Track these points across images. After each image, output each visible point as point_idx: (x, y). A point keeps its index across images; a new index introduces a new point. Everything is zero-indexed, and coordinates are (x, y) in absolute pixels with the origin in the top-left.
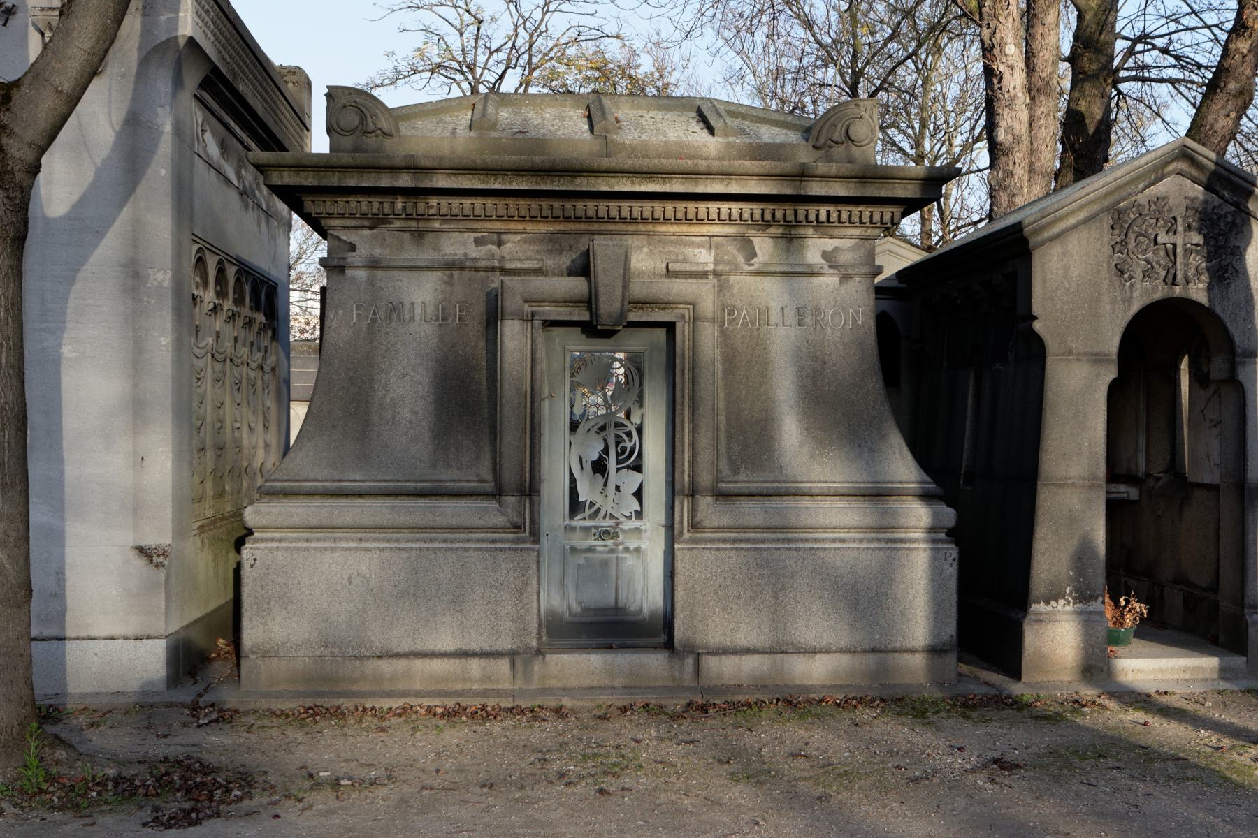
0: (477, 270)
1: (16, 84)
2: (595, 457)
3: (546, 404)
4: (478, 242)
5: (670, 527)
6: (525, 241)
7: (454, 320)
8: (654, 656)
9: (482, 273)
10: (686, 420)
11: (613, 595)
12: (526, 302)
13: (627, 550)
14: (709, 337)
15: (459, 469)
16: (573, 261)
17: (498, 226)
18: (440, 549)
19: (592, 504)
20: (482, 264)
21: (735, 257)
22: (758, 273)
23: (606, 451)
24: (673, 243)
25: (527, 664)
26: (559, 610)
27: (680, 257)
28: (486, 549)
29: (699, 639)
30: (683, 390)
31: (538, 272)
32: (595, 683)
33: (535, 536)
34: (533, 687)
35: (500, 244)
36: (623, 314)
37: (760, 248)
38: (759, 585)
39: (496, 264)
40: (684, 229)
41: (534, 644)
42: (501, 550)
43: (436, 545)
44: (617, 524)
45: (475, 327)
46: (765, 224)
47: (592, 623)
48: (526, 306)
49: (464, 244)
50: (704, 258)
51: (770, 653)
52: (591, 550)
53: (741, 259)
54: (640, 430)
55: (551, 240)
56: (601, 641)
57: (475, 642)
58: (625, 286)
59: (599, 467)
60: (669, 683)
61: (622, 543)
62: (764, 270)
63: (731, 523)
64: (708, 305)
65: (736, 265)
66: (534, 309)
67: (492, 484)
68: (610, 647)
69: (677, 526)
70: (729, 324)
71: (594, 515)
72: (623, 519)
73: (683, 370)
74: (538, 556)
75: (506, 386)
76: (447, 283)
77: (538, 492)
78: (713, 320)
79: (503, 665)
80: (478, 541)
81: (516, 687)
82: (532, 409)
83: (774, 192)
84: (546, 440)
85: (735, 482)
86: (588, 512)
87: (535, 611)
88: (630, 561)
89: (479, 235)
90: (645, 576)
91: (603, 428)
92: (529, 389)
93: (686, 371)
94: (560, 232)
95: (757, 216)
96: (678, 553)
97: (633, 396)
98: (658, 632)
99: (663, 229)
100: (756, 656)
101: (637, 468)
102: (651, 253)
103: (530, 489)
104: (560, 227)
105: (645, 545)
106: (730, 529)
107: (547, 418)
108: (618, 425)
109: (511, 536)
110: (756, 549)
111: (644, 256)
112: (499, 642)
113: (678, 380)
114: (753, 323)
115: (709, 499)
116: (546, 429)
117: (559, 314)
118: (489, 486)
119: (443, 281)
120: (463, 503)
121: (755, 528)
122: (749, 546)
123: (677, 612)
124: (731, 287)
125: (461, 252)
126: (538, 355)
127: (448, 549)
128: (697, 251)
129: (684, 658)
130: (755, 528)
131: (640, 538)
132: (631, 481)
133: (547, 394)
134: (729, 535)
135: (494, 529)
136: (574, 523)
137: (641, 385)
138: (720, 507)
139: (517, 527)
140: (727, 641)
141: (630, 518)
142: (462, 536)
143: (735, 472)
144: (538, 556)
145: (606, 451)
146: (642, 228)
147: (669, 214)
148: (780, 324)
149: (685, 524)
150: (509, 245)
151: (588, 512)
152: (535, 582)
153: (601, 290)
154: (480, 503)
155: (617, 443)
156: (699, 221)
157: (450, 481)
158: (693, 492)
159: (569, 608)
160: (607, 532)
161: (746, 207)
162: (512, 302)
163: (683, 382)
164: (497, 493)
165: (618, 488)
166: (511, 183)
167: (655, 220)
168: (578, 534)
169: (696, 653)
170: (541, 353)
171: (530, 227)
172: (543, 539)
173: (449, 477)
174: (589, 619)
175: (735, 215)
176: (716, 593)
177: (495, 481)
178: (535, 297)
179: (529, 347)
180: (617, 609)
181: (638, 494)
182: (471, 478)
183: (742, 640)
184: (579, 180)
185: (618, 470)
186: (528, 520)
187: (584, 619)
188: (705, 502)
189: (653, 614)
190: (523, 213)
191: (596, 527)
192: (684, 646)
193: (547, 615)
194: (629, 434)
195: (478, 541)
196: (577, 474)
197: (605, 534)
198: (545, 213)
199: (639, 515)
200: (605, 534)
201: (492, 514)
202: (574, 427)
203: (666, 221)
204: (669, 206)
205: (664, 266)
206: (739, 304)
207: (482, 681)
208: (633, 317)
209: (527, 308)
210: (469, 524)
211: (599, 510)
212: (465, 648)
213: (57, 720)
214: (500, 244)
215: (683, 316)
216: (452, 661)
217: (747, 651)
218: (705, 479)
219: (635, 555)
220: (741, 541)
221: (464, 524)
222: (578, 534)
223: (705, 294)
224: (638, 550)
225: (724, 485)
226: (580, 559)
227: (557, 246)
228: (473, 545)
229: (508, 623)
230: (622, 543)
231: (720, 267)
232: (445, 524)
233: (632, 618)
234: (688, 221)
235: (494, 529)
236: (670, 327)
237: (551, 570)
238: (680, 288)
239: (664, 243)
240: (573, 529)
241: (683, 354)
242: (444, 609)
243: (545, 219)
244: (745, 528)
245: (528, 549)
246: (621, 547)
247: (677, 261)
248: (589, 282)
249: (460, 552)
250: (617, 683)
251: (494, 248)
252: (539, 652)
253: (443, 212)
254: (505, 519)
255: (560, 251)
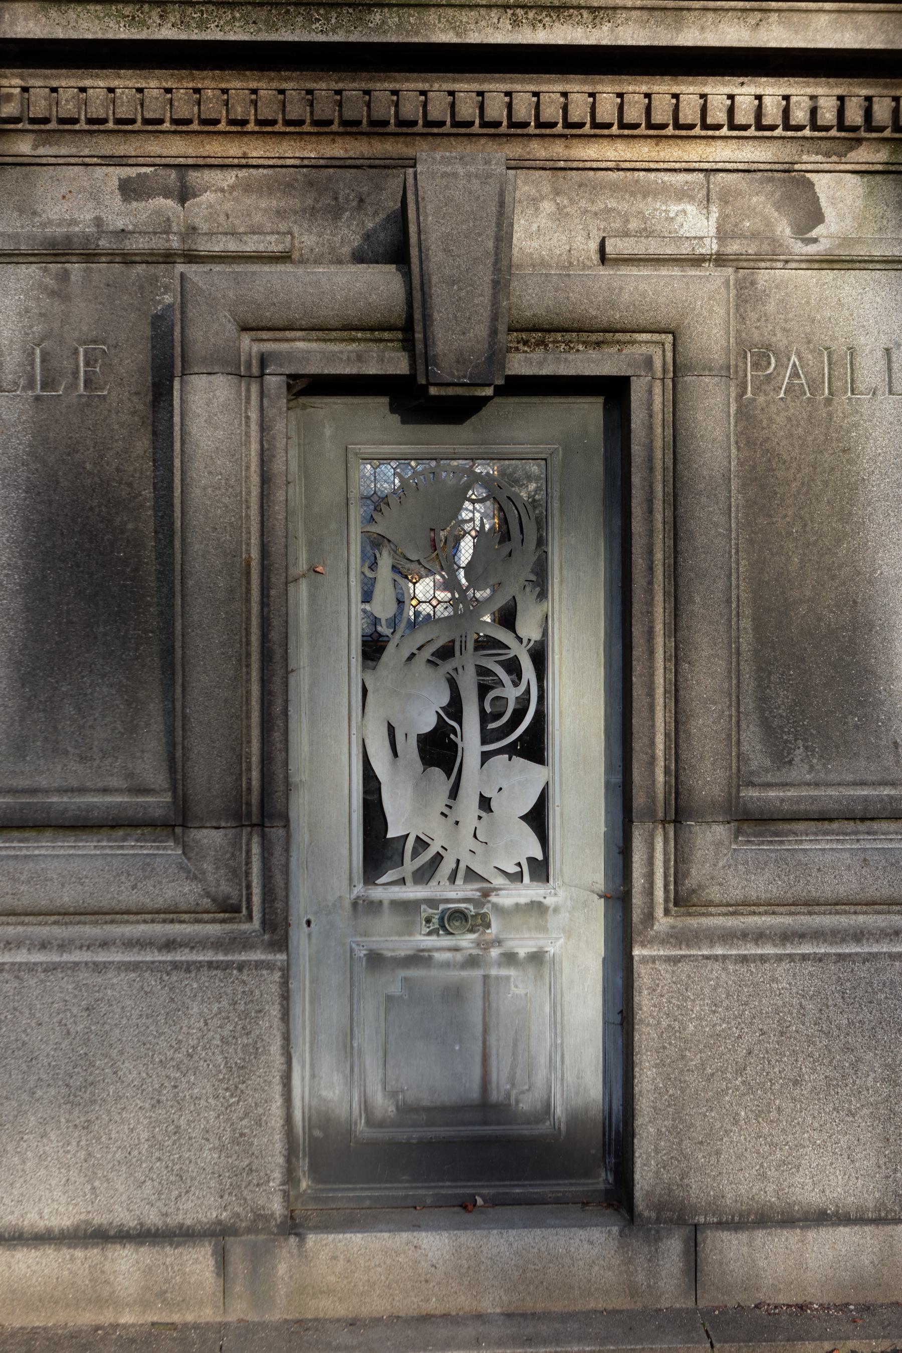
0: (128, 259)
1: (514, 631)
2: (428, 724)
3: (302, 590)
4: (130, 190)
5: (619, 898)
6: (247, 188)
7: (74, 385)
8: (582, 1234)
9: (140, 269)
10: (659, 628)
11: (477, 1073)
12: (245, 329)
13: (510, 958)
14: (713, 413)
15: (82, 759)
16: (367, 237)
17: (178, 148)
18: (31, 968)
19: (422, 844)
20: (140, 244)
21: (768, 224)
22: (830, 262)
23: (455, 709)
24: (614, 188)
25: (259, 1259)
26: (341, 1112)
27: (633, 225)
28: (151, 966)
29: (698, 1189)
30: (650, 552)
31: (284, 258)
32: (433, 1306)
33: (277, 931)
34: (275, 1316)
35: (184, 195)
36: (495, 355)
37: (833, 202)
38: (848, 1049)
39: (175, 243)
40: (643, 151)
41: (277, 1207)
42: (188, 967)
43: (21, 956)
44: (486, 894)
45: (123, 399)
46: (848, 134)
47: (428, 1145)
48: (246, 340)
49: (95, 196)
50: (696, 224)
51: (878, 1221)
52: (419, 959)
53: (784, 229)
54: (539, 656)
55: (311, 184)
56: (448, 1189)
57: (125, 1202)
58: (500, 285)
59: (439, 750)
60: (621, 1303)
61: (499, 942)
62: (843, 252)
63: (776, 891)
64: (712, 330)
65: (774, 241)
66: (268, 347)
67: (167, 798)
68: (466, 1205)
69: (637, 900)
70: (757, 390)
71: (426, 874)
72: (499, 881)
73: (650, 501)
74: (285, 982)
75: (197, 547)
76: (53, 294)
77: (285, 820)
78: (727, 372)
79: (198, 1262)
80: (130, 944)
81: (232, 1318)
82: (264, 603)
83: (877, 44)
84: (302, 682)
85: (784, 785)
86: (410, 865)
87: (277, 1121)
88: (519, 986)
89: (132, 172)
90: (556, 1023)
91: (446, 653)
92: (255, 554)
93: (658, 505)
94: (334, 164)
95: (828, 116)
96: (642, 972)
97: (521, 570)
98: (588, 1166)
99: (590, 151)
100: (844, 1231)
101: (533, 748)
102: (560, 214)
103: (262, 810)
104: (336, 149)
105: (554, 946)
106: (772, 905)
107: (304, 627)
108: (487, 644)
109: (213, 930)
110: (841, 957)
111: (543, 221)
112: (187, 1205)
113: (638, 526)
114: (814, 386)
115: (720, 831)
116: (302, 655)
117: (331, 358)
118: (157, 803)
119: (43, 288)
120: (89, 846)
121: (838, 904)
122: (823, 949)
123: (639, 1121)
124: (760, 298)
125: (87, 216)
126: (278, 466)
127: (51, 968)
128: (674, 208)
129: (658, 1239)
130: (838, 904)
131: (543, 929)
132: (518, 783)
133: (303, 565)
134: (769, 920)
135: (170, 913)
136: (377, 893)
137: (541, 542)
138: (750, 849)
139: (229, 909)
140: (768, 1194)
141: (519, 877)
142: (89, 931)
143: (782, 759)
144: (285, 982)
145: (455, 709)
146: (539, 150)
147: (607, 111)
148: (883, 387)
149: (659, 894)
150: (208, 197)
151: (410, 865)
152: (276, 1048)
153: (439, 292)
154: (134, 848)
155: (483, 690)
156: (682, 130)
157: (61, 791)
158: (679, 813)
159: (367, 1107)
160: (459, 916)
161: (801, 92)
162: (210, 330)
163: (651, 532)
164: (176, 822)
165: (485, 803)
166: (202, 25)
167: (572, 129)
168: (388, 920)
169: (691, 1224)
170: (288, 461)
171: (257, 150)
172: (299, 937)
173: (56, 780)
174: (415, 1135)
175: (772, 112)
176: (741, 1070)
177: (174, 789)
178: (268, 315)
179: (255, 446)
180: (487, 1108)
181: (538, 818)
182: (114, 782)
183: (807, 1191)
184: (377, 17)
185: (486, 757)
186: (256, 890)
187: (402, 1135)
188: (710, 838)
189: (576, 1119)
190: (239, 112)
191: (432, 903)
192: (660, 1207)
193: (310, 1124)
194: (513, 667)
195: (130, 944)
196: (381, 767)
197: (453, 919)
198: (294, 112)
199: (540, 869)
200: (453, 919)
201: (158, 874)
202: (373, 648)
203: (599, 129)
204: (607, 90)
205: (594, 246)
206: (779, 340)
207: (144, 1304)
208: (522, 364)
209: (248, 345)
210: (105, 902)
211: (438, 858)
212: (100, 1219)
213: (538, 596)
214: (184, 195)
215: (649, 362)
216: (66, 1253)
217: (821, 1218)
218: (708, 780)
219: (531, 971)
220: (801, 936)
221: (92, 903)
222: (388, 920)
223: (706, 307)
224: (537, 958)
225: (753, 793)
226: (393, 983)
227: (327, 200)
228: (116, 956)
229: (209, 1156)
230: (499, 942)
231: (733, 247)
232: (44, 903)
233: (526, 1131)
234: (654, 130)
235: (170, 913)
236: (614, 391)
237: (319, 1009)
238: (643, 290)
239: (595, 189)
240: (374, 907)
241: (650, 459)
242: (43, 1122)
243: (294, 128)
244: (810, 904)
245: (259, 965)
246: (495, 952)
247: (627, 234)
248: (407, 275)
249: (83, 976)
250: (489, 1305)
251: (168, 204)
252: (293, 1226)
253: (39, 109)
254: (197, 888)
255: (335, 212)
